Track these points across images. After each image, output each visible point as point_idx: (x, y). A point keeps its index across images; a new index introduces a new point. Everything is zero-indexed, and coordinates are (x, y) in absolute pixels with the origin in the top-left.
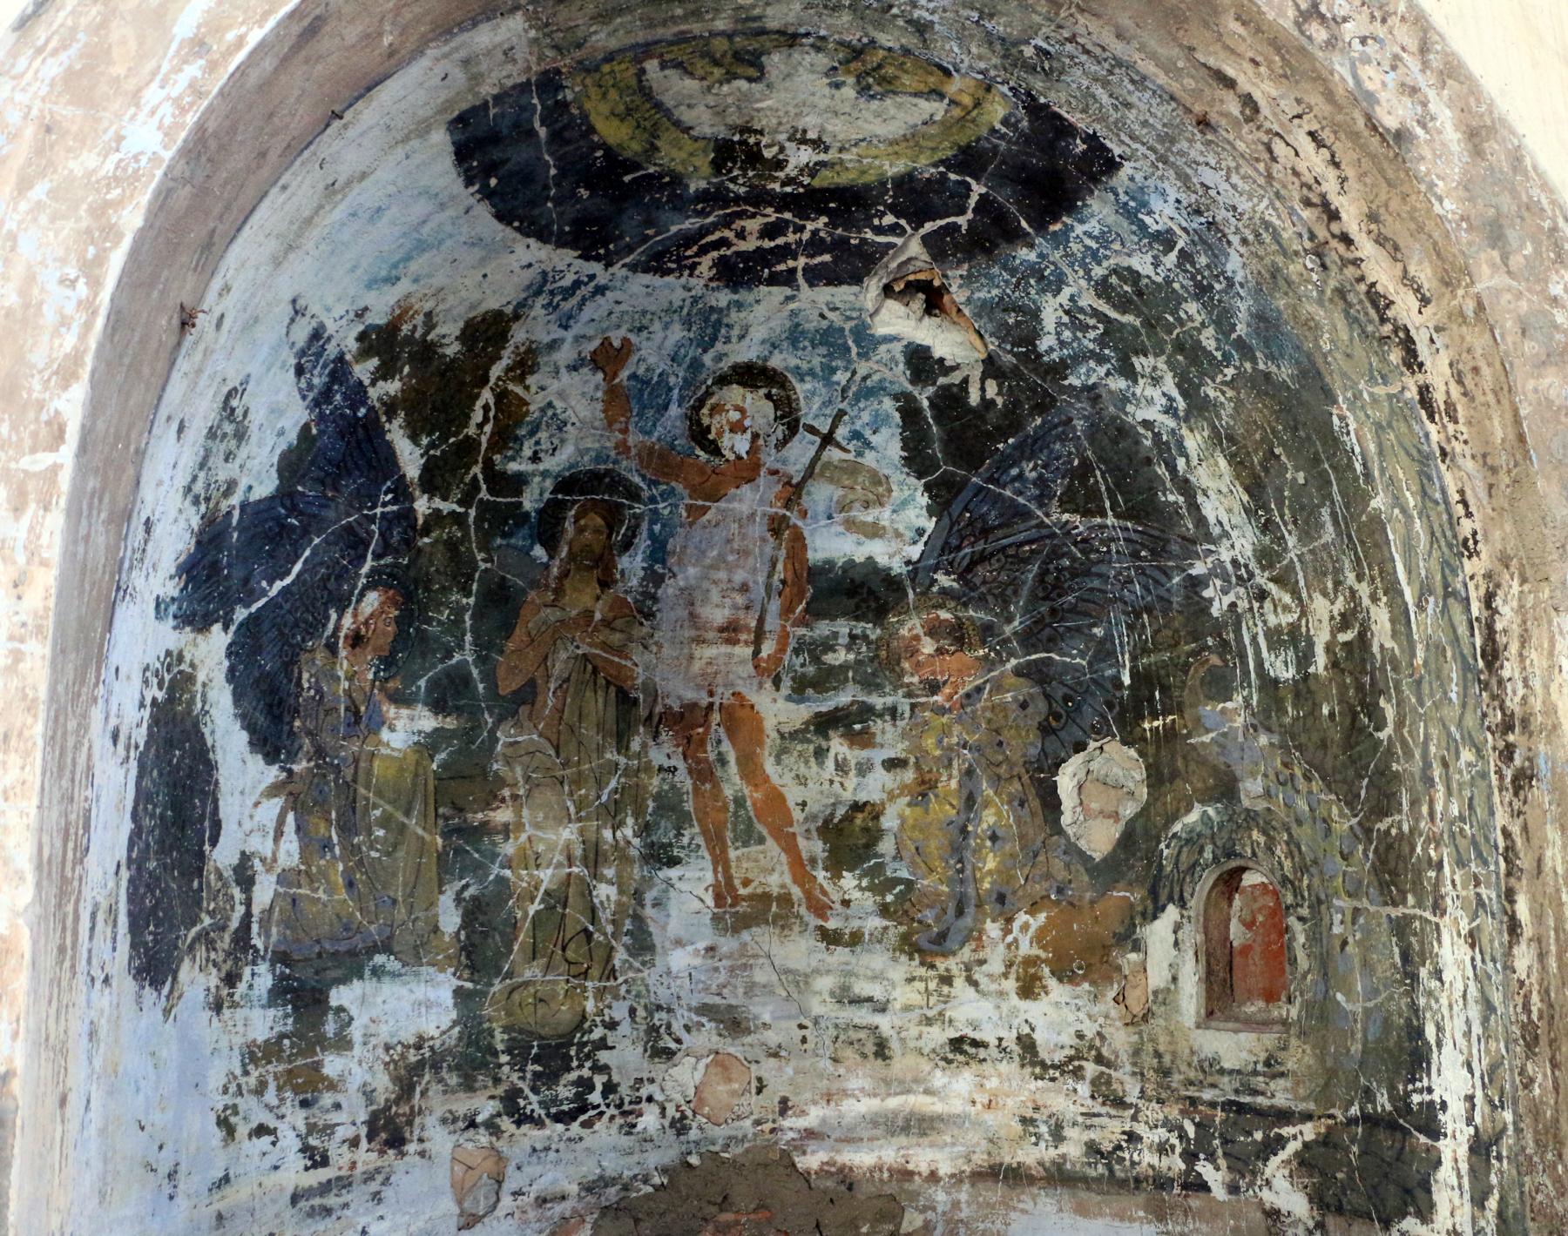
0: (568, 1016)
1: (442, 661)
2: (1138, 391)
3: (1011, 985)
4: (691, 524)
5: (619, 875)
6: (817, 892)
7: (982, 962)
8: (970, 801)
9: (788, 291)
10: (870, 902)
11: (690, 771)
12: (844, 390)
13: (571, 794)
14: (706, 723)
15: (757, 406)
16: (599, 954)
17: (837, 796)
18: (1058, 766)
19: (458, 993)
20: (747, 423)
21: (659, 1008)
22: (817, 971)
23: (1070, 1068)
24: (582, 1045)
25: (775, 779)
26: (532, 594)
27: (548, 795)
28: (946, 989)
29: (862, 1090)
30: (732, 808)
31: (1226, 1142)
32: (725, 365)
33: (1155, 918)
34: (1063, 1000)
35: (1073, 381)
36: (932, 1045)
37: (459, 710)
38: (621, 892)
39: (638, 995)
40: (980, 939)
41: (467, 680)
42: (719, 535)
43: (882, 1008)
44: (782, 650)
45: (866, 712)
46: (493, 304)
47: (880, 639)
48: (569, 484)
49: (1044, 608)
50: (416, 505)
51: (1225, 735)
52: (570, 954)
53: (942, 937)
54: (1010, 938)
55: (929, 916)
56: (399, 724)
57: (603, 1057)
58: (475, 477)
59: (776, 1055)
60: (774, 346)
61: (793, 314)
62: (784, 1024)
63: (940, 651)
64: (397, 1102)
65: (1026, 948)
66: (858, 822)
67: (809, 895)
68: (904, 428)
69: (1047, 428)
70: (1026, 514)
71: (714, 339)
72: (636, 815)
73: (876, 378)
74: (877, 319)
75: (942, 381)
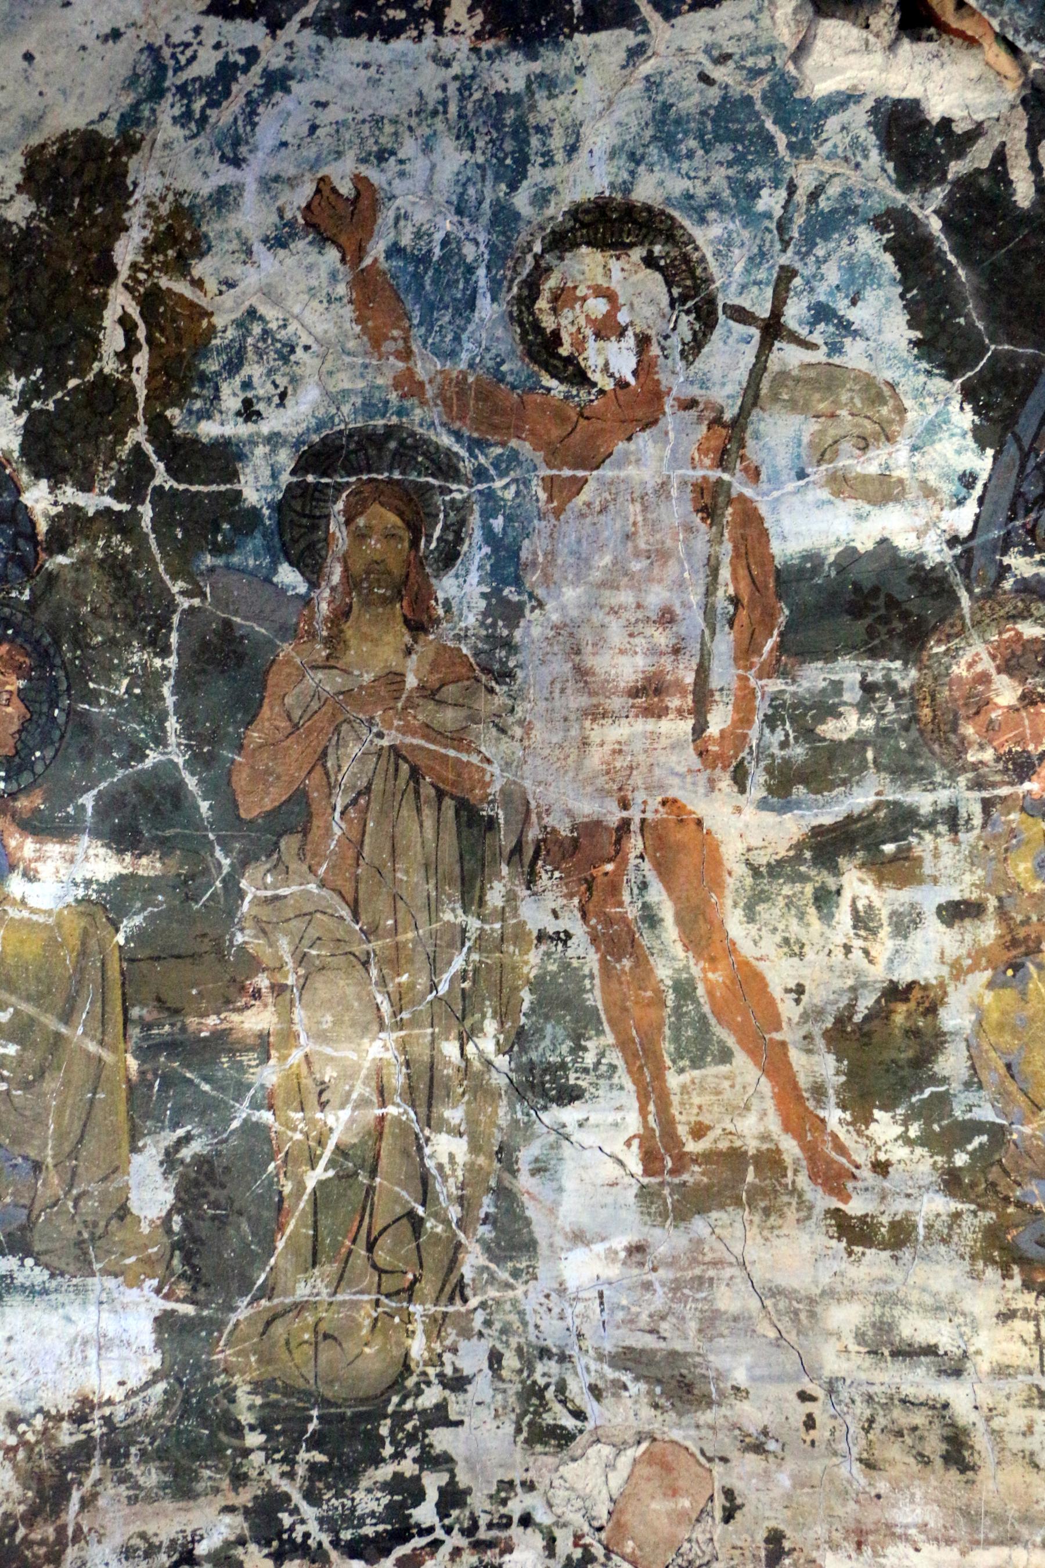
0: (378, 1366)
1: (124, 763)
4: (558, 512)
5: (471, 1120)
9: (629, 38)
10: (925, 1166)
11: (594, 940)
12: (782, 227)
13: (383, 981)
14: (618, 853)
15: (630, 282)
16: (434, 1256)
17: (857, 973)
19: (164, 1322)
20: (623, 318)
21: (544, 1353)
24: (400, 1418)
25: (747, 949)
26: (286, 649)
27: (342, 985)
29: (923, 1527)
30: (670, 998)
32: (557, 209)
37: (165, 846)
38: (475, 1148)
39: (505, 1331)
41: (176, 794)
42: (611, 527)
43: (955, 1370)
44: (745, 721)
45: (904, 820)
46: (70, 117)
47: (917, 686)
48: (322, 455)
50: (28, 498)
52: (382, 1256)
56: (45, 870)
57: (441, 1439)
58: (137, 447)
59: (758, 1448)
60: (636, 159)
61: (652, 84)
62: (772, 1390)
64: (30, 1518)
66: (899, 1019)
67: (812, 1152)
68: (906, 282)
71: (522, 162)
72: (502, 1016)
73: (834, 190)
74: (810, 63)
75: (956, 168)
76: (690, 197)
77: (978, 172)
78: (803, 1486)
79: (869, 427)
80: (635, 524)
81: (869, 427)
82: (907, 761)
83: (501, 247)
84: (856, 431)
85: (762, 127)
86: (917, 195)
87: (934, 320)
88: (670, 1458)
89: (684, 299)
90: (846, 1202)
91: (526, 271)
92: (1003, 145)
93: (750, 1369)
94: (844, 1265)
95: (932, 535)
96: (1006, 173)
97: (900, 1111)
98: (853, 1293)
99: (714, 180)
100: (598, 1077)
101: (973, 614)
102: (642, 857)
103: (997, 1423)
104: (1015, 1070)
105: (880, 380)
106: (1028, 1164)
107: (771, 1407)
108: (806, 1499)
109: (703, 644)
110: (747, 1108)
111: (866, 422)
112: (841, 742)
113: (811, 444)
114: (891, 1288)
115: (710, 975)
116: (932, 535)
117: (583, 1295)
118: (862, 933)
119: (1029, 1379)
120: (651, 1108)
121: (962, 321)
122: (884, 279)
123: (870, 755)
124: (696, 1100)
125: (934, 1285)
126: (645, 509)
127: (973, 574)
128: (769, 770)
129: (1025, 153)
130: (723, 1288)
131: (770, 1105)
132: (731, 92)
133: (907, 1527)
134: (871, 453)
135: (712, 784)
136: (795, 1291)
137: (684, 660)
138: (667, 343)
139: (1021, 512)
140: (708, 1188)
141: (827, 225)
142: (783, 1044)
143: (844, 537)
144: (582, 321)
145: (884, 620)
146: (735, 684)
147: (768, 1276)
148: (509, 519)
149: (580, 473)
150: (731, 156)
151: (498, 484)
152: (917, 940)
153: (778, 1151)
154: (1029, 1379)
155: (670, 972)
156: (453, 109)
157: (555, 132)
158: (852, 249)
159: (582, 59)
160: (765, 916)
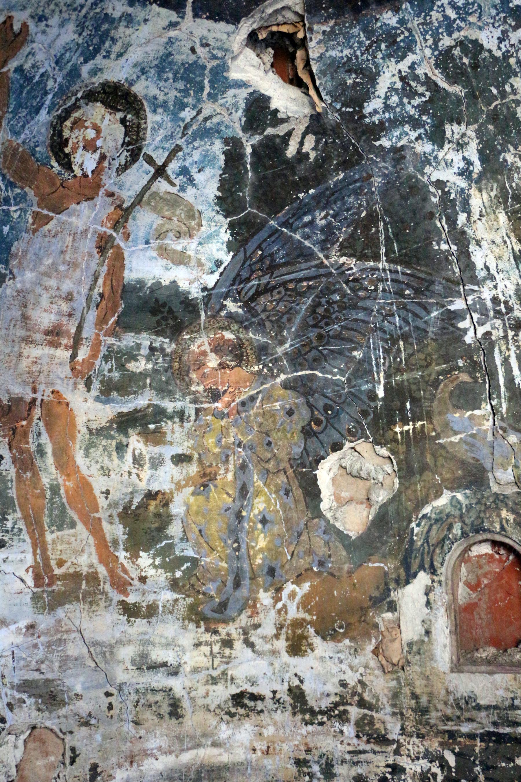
2: (441, 155)
3: (281, 644)
4: (35, 231)
6: (119, 571)
7: (257, 626)
8: (243, 491)
9: (173, 16)
10: (163, 578)
11: (14, 462)
12: (186, 127)
14: (28, 417)
15: (106, 125)
17: (134, 486)
18: (318, 462)
20: (99, 143)
22: (120, 642)
23: (336, 712)
25: (84, 471)
28: (227, 651)
29: (160, 748)
30: (48, 493)
31: (486, 768)
32: (98, 80)
33: (407, 582)
34: (327, 655)
35: (385, 142)
36: (217, 702)
40: (254, 606)
42: (57, 245)
43: (175, 672)
44: (94, 356)
45: (160, 414)
47: (174, 352)
49: (312, 334)
51: (473, 436)
53: (223, 606)
54: (279, 605)
55: (211, 588)
59: (87, 724)
60: (143, 71)
61: (170, 42)
62: (93, 693)
63: (222, 366)
65: (294, 613)
66: (152, 508)
67: (112, 572)
68: (225, 170)
69: (347, 182)
70: (307, 255)
71: (97, 51)
73: (215, 120)
75: (270, 131)
76: (155, 98)
77: (278, 136)
78: (107, 738)
79: (184, 228)
80: (67, 247)
81: (184, 228)
82: (164, 386)
83: (65, 88)
84: (178, 229)
85: (203, 81)
86: (248, 135)
87: (229, 190)
88: (44, 737)
89: (129, 144)
90: (127, 597)
91: (69, 104)
92: (294, 129)
93: (83, 684)
94: (126, 627)
95: (196, 284)
96: (288, 140)
97: (151, 552)
98: (130, 641)
99: (169, 95)
100: (13, 535)
101: (205, 323)
102: (39, 419)
103: (193, 694)
104: (203, 533)
105: (196, 209)
106: (208, 575)
107: (93, 702)
108: (108, 745)
109: (83, 314)
110: (83, 551)
111: (183, 226)
112: (136, 373)
113: (156, 230)
114: (147, 637)
115: (67, 483)
116: (196, 284)
117: (5, 654)
118: (137, 466)
119: (207, 672)
120: (38, 551)
121: (241, 194)
122: (217, 166)
123: (148, 381)
124: (59, 547)
125: (166, 634)
126: (74, 240)
127: (209, 306)
128: (102, 382)
129: (300, 136)
130: (71, 644)
131: (93, 549)
132: (200, 61)
133: (152, 749)
134: (181, 241)
135: (75, 385)
136: (104, 642)
137: (72, 320)
138: (113, 162)
139: (237, 283)
140: (65, 592)
141: (205, 133)
142: (99, 519)
143: (157, 276)
144: (81, 138)
145: (165, 319)
146: (93, 337)
147: (92, 636)
148: (12, 228)
149: (51, 214)
150: (183, 88)
151: (13, 208)
152: (161, 471)
153: (96, 573)
154: (207, 672)
155: (48, 480)
156: (84, 11)
157: (118, 43)
158: (210, 148)
159: (150, 17)
160: (93, 455)
